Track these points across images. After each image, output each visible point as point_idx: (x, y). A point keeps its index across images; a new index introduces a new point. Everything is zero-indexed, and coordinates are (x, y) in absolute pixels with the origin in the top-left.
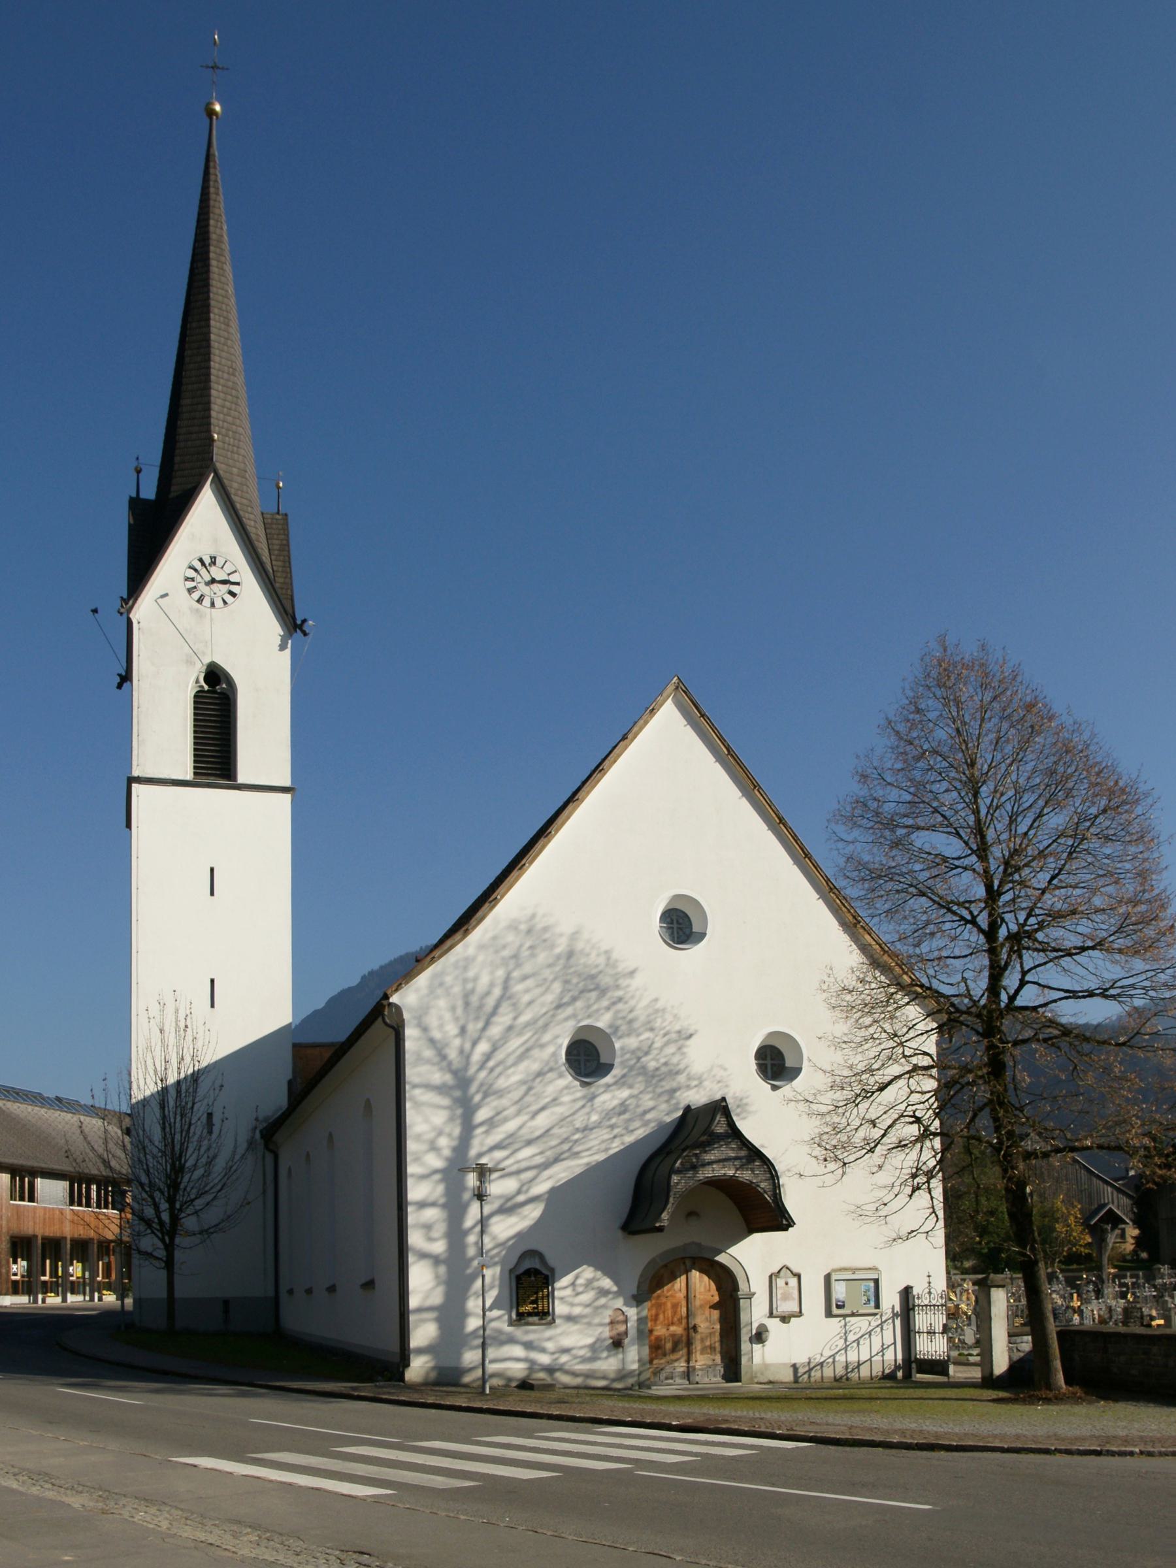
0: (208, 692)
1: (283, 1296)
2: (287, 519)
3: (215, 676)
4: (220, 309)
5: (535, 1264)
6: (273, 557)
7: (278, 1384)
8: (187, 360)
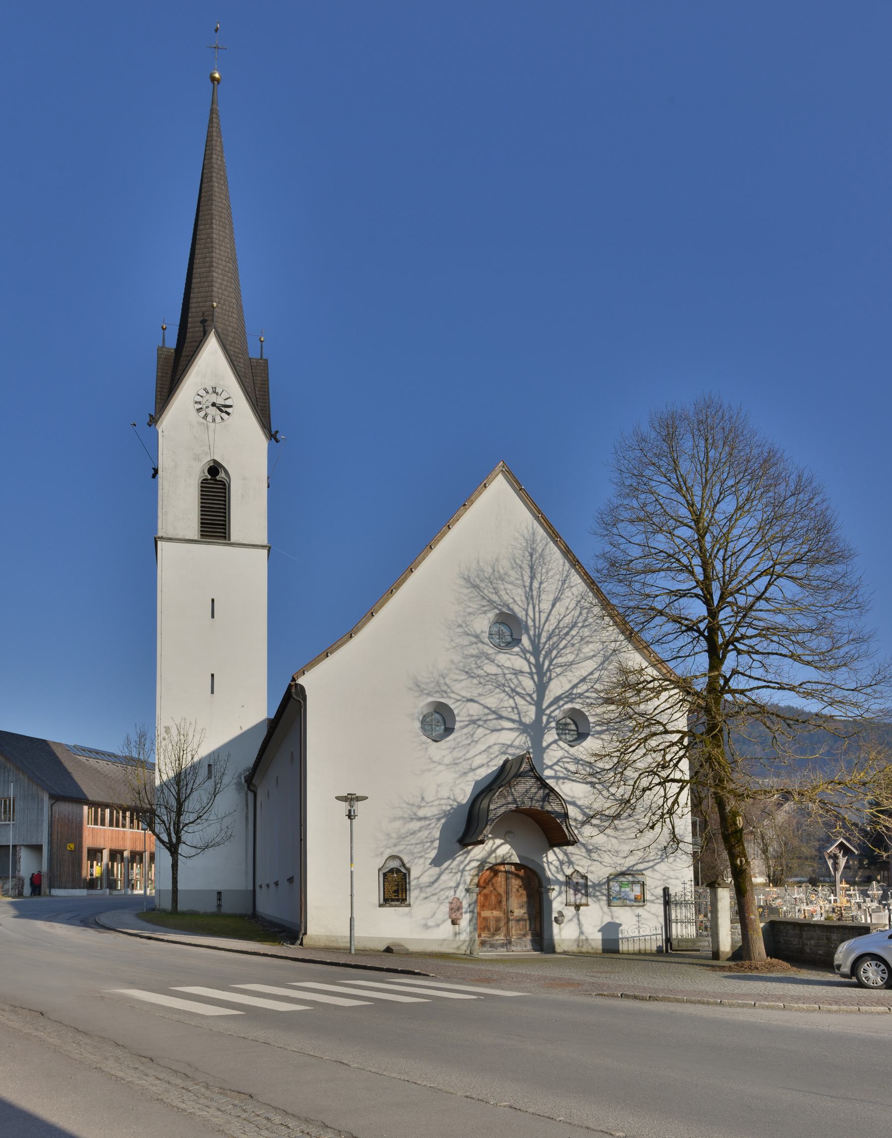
0: (211, 479)
1: (258, 889)
2: (267, 363)
3: (215, 469)
4: (221, 217)
5: (395, 864)
6: (256, 389)
7: (125, 930)
8: (197, 251)
